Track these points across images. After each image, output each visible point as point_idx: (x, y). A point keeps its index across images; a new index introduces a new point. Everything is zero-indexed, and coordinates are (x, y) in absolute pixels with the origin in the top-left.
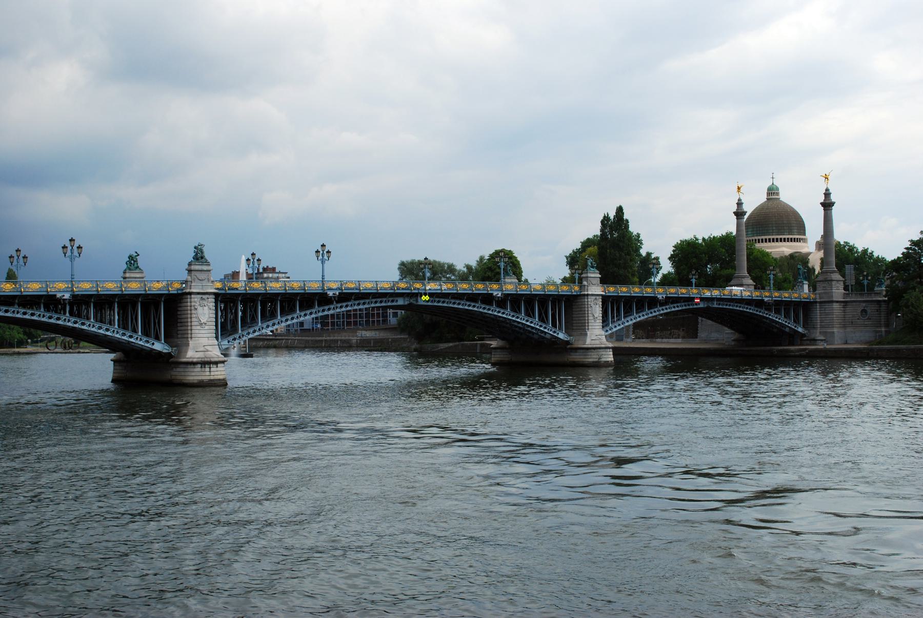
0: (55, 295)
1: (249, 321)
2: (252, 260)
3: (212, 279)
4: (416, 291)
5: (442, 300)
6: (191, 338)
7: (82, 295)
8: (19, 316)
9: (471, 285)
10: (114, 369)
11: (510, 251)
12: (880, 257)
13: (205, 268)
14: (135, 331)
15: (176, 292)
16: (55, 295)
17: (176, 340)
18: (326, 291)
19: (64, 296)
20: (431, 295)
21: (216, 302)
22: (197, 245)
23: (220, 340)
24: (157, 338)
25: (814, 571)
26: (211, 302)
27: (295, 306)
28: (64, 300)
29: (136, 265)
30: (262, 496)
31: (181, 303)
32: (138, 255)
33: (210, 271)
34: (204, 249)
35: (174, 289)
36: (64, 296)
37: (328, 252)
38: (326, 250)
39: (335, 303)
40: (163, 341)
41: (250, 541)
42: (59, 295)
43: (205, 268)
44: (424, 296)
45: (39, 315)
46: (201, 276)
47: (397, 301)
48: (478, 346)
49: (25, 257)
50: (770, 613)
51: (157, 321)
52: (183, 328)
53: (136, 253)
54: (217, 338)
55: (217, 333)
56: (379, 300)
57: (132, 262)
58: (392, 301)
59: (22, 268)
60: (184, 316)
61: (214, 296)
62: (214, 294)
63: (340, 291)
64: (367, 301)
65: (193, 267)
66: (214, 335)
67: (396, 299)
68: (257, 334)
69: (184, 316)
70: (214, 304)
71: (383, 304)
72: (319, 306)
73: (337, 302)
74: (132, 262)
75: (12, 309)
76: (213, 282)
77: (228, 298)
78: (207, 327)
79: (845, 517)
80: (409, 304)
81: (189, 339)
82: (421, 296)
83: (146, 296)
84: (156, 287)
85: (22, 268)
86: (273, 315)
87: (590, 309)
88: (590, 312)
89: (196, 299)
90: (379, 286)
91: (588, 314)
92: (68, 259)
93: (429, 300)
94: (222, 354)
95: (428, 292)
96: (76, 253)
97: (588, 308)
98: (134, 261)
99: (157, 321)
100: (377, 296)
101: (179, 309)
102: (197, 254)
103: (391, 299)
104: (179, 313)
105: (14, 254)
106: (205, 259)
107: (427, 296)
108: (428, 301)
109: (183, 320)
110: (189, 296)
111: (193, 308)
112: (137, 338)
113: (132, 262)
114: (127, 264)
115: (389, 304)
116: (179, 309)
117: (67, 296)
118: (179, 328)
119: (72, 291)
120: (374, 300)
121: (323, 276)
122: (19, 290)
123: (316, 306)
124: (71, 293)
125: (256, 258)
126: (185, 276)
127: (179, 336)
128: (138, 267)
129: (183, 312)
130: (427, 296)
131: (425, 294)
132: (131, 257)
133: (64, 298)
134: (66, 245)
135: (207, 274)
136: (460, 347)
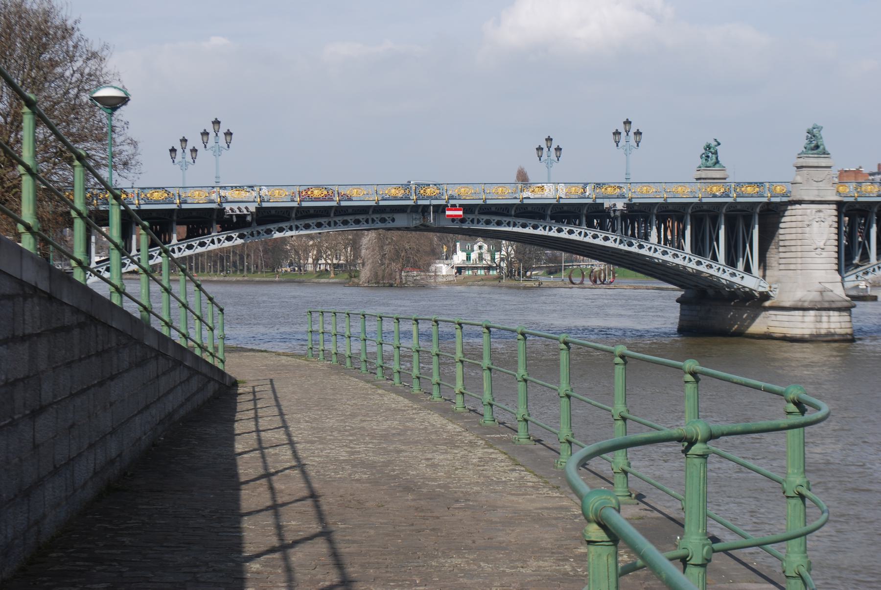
0: (603, 204)
5: (497, 218)
7: (640, 203)
10: (681, 315)
13: (823, 162)
16: (603, 204)
21: (839, 216)
23: (843, 272)
25: (752, 516)
26: (830, 212)
28: (615, 211)
30: (853, 509)
32: (719, 144)
41: (96, 413)
42: (607, 204)
43: (823, 162)
49: (638, 133)
54: (839, 271)
55: (839, 264)
61: (834, 206)
66: (836, 267)
70: (836, 219)
74: (710, 154)
79: (730, 460)
83: (733, 206)
84: (750, 195)
92: (544, 164)
94: (847, 296)
96: (632, 142)
105: (621, 129)
108: (463, 221)
112: (719, 269)
117: (620, 205)
126: (791, 174)
132: (708, 147)
134: (542, 146)
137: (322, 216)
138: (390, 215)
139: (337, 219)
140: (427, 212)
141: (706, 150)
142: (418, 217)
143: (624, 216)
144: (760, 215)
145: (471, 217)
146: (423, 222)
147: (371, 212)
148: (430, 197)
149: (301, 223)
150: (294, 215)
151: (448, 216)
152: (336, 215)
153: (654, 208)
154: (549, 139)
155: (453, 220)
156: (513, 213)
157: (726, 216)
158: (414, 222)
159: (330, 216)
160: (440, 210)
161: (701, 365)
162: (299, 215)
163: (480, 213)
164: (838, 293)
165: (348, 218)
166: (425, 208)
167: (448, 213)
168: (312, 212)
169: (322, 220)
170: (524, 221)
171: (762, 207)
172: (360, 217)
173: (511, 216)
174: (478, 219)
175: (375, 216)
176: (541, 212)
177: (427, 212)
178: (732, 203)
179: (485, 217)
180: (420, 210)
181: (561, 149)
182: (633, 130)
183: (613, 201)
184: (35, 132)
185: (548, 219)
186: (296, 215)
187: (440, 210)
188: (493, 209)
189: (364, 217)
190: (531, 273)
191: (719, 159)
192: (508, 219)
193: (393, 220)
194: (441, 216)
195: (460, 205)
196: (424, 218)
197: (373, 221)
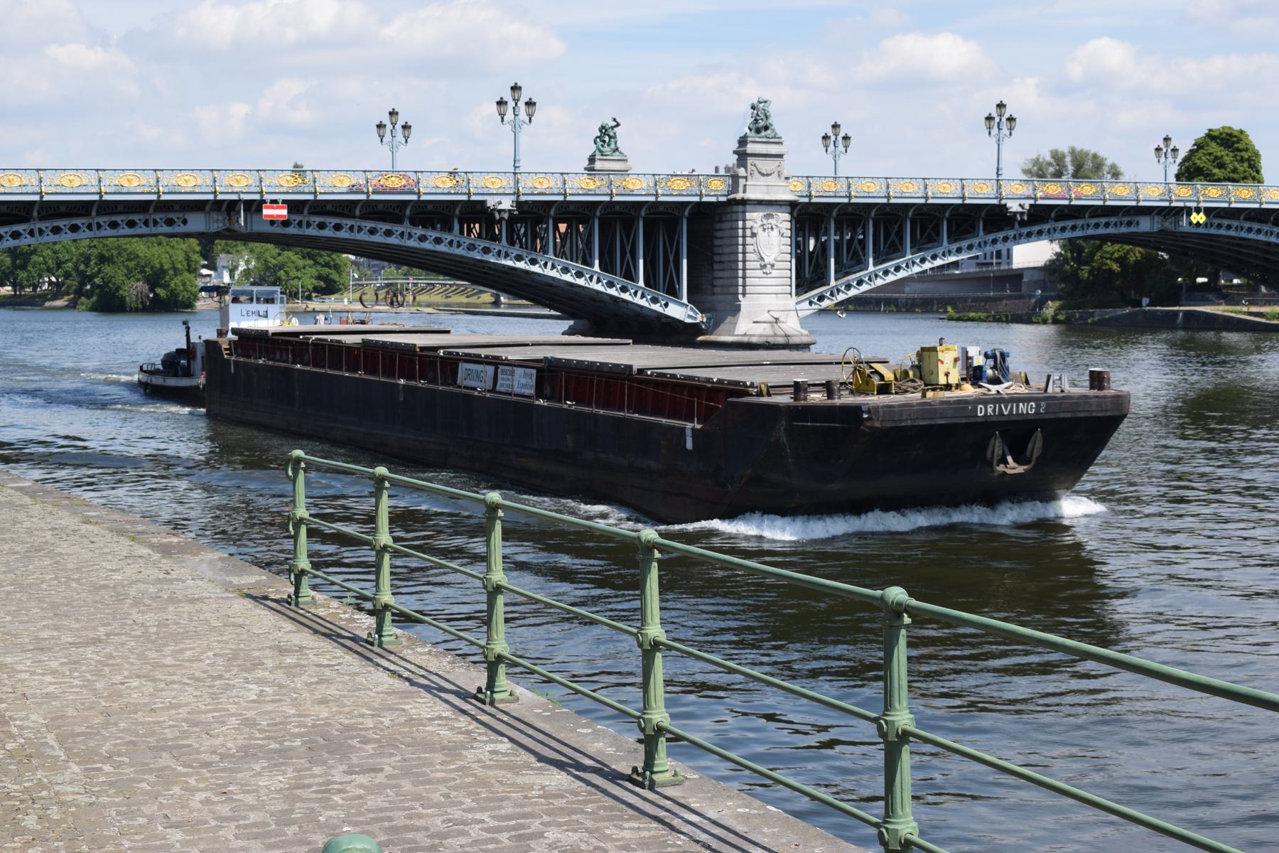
0: (484, 202)
1: (851, 261)
2: (833, 138)
3: (786, 173)
4: (1181, 204)
5: (334, 221)
6: (744, 294)
8: (412, 243)
9: (1228, 190)
11: (1241, 132)
12: (1041, 160)
13: (773, 149)
14: (630, 275)
15: (714, 199)
17: (709, 298)
18: (1003, 202)
19: (500, 203)
20: (1208, 211)
22: (755, 102)
24: (673, 292)
26: (783, 220)
27: (938, 232)
28: (500, 211)
29: (613, 146)
31: (721, 221)
32: (618, 125)
33: (780, 156)
34: (772, 110)
35: (716, 191)
36: (500, 203)
37: (1011, 119)
38: (1007, 115)
39: (1016, 225)
40: (685, 300)
42: (491, 202)
44: (1194, 214)
45: (451, 243)
46: (765, 165)
47: (1138, 223)
48: (1181, 314)
50: (247, 719)
51: (671, 258)
52: (726, 274)
53: (615, 120)
56: (1103, 220)
57: (607, 139)
58: (1129, 224)
59: (1006, 139)
60: (727, 250)
61: (789, 209)
62: (792, 205)
63: (1032, 202)
64: (1080, 222)
65: (751, 148)
67: (1136, 219)
68: (865, 287)
69: (727, 250)
71: (1101, 231)
72: (987, 232)
73: (414, 223)
75: (398, 229)
76: (787, 178)
77: (662, 213)
78: (774, 273)
80: (1162, 231)
81: (740, 297)
82: (1189, 214)
85: (1006, 139)
86: (859, 263)
87: (749, 240)
88: (749, 248)
89: (754, 218)
90: (1141, 192)
91: (744, 253)
93: (1206, 224)
95: (1203, 205)
97: (744, 237)
98: (610, 137)
99: (671, 258)
100: (1099, 212)
101: (719, 234)
102: (756, 120)
103: (1126, 219)
104: (717, 242)
106: (773, 131)
107: (1202, 214)
108: (286, 223)
109: (725, 258)
110: (740, 208)
111: (748, 233)
113: (607, 139)
114: (595, 142)
115: (1111, 230)
116: (719, 234)
117: (507, 204)
118: (718, 274)
119: (517, 194)
120: (1093, 221)
121: (998, 170)
122: (155, 190)
123: (981, 233)
124: (514, 198)
125: (842, 134)
127: (717, 290)
128: (617, 150)
129: (726, 241)
130: (1202, 214)
131: (1198, 210)
132: (603, 129)
133: (500, 207)
135: (777, 163)
136: (1140, 317)
137: (79, 215)
138: (180, 215)
139: (101, 220)
140: (234, 210)
141: (601, 131)
142: (221, 218)
143: (513, 220)
144: (688, 220)
145: (298, 218)
146: (228, 225)
147: (151, 210)
148: (237, 186)
149: (65, 223)
150: (35, 214)
151: (267, 216)
152: (155, 211)
153: (455, 209)
154: (393, 113)
155: (272, 223)
156: (357, 213)
157: (644, 220)
158: (216, 225)
159: (90, 215)
160: (254, 208)
161: (339, 341)
162: (44, 213)
163: (310, 213)
164: (792, 326)
165: (118, 218)
166: (232, 206)
167: (266, 212)
168: (63, 209)
169: (78, 221)
170: (373, 225)
171: (691, 209)
172: (136, 217)
173: (354, 217)
174: (308, 222)
175: (158, 217)
176: (397, 212)
177: (234, 210)
178: (884, 204)
179: (318, 219)
180: (224, 208)
181: (535, 104)
182: (401, 122)
183: (497, 199)
184: (135, 311)
185: (407, 223)
186: (39, 213)
187: (254, 207)
188: (329, 207)
189: (142, 216)
190: (924, 396)
191: (618, 145)
192: (349, 222)
193: (185, 222)
194: (255, 217)
195: (284, 202)
196: (230, 219)
197: (155, 223)
